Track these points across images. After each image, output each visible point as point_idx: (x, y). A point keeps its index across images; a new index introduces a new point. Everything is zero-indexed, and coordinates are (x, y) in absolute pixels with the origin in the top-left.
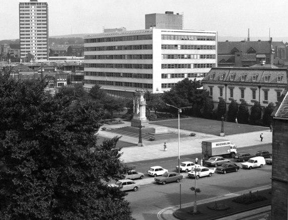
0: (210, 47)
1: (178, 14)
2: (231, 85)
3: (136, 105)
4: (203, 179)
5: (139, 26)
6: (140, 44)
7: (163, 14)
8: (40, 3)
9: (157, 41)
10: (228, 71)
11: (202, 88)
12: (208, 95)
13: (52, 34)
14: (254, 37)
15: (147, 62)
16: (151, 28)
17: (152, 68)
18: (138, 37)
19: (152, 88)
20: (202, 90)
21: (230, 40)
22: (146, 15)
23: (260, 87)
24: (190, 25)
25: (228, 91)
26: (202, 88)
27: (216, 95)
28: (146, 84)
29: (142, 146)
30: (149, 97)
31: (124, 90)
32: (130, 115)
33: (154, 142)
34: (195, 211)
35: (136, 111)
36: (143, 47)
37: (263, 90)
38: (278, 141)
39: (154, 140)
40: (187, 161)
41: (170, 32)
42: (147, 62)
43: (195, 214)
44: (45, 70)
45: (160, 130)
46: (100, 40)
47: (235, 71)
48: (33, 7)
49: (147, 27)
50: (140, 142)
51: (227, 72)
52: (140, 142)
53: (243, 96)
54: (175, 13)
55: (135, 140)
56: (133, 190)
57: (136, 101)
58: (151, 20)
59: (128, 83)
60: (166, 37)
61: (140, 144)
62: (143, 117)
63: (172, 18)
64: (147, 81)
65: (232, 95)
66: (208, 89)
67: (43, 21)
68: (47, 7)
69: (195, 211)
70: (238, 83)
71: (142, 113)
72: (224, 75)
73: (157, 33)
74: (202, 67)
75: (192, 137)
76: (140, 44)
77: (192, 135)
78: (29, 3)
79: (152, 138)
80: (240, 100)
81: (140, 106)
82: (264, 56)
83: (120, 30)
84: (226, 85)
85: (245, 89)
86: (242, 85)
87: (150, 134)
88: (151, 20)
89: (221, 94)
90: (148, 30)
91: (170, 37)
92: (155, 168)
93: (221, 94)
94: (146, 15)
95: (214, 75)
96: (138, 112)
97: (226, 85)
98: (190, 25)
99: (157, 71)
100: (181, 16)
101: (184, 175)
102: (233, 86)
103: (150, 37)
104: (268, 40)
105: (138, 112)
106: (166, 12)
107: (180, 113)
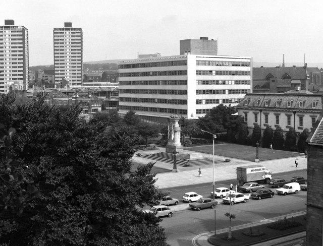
0: (245, 73)
1: (212, 40)
3: (171, 131)
5: (174, 52)
6: (174, 70)
8: (75, 29)
9: (192, 67)
11: (236, 114)
13: (86, 59)
14: (289, 63)
15: (182, 87)
16: (186, 54)
17: (186, 94)
19: (186, 113)
20: (237, 116)
22: (181, 41)
23: (295, 113)
24: (225, 50)
25: (263, 116)
27: (251, 121)
29: (176, 172)
30: (184, 123)
32: (165, 141)
33: (188, 168)
34: (230, 237)
35: (171, 136)
41: (205, 58)
42: (182, 87)
44: (79, 96)
45: (195, 156)
46: (134, 66)
47: (270, 97)
48: (67, 33)
49: (182, 53)
50: (175, 167)
51: (262, 98)
52: (175, 167)
53: (278, 122)
54: (209, 39)
55: (170, 166)
56: (168, 216)
58: (186, 46)
61: (174, 170)
62: (178, 143)
64: (182, 107)
66: (243, 115)
67: (77, 46)
68: (81, 33)
71: (177, 139)
72: (259, 101)
73: (192, 59)
74: (237, 93)
76: (174, 70)
77: (227, 161)
78: (63, 29)
79: (187, 164)
81: (175, 132)
82: (299, 82)
83: (154, 56)
84: (261, 111)
85: (280, 114)
86: (277, 110)
88: (186, 46)
89: (256, 120)
90: (182, 56)
91: (204, 63)
92: (190, 194)
93: (256, 120)
94: (181, 41)
97: (261, 111)
98: (225, 50)
99: (192, 97)
100: (216, 41)
102: (279, 113)
103: (185, 63)
104: (303, 65)
106: (201, 38)
107: (215, 139)
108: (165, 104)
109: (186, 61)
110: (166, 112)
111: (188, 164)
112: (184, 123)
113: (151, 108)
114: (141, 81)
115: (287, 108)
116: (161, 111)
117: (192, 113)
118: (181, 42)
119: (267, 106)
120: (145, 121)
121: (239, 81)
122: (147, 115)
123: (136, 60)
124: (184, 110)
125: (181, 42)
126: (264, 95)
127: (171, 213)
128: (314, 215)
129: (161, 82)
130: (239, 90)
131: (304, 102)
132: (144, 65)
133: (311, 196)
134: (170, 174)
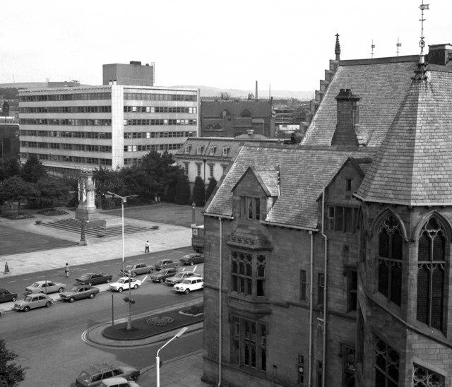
2: (211, 160)
3: (82, 189)
4: (33, 312)
5: (94, 79)
6: (98, 102)
7: (124, 65)
9: (117, 103)
10: (208, 142)
11: (175, 164)
12: (181, 175)
14: (263, 94)
15: (104, 129)
16: (111, 83)
17: (111, 138)
18: (94, 96)
19: (111, 164)
20: (175, 167)
21: (234, 95)
22: (104, 66)
24: (165, 80)
25: (208, 168)
26: (175, 164)
27: (192, 174)
28: (104, 160)
29: (85, 245)
30: (103, 179)
31: (74, 168)
32: (74, 203)
33: (102, 239)
34: (129, 327)
35: (81, 198)
36: (85, 109)
37: (209, 165)
38: (210, 241)
39: (102, 236)
40: (41, 280)
41: (135, 89)
42: (104, 129)
43: (130, 330)
45: (112, 221)
46: (43, 98)
47: (216, 143)
49: (105, 82)
50: (83, 239)
51: (206, 144)
52: (83, 239)
55: (76, 237)
56: (46, 306)
57: (82, 185)
58: (111, 72)
59: (80, 158)
60: (138, 96)
61: (82, 243)
62: (91, 205)
63: (140, 72)
64: (105, 156)
65: (212, 173)
66: (183, 166)
69: (129, 327)
70: (219, 159)
71: (90, 200)
72: (203, 148)
73: (117, 90)
74: (179, 136)
75: (155, 231)
76: (98, 102)
77: (156, 228)
79: (101, 233)
80: (209, 179)
81: (87, 191)
83: (70, 84)
84: (205, 161)
85: (214, 165)
87: (99, 228)
88: (111, 72)
89: (199, 172)
90: (105, 86)
91: (137, 97)
93: (199, 172)
94: (104, 66)
95: (190, 148)
96: (84, 200)
97: (205, 161)
98: (165, 80)
99: (117, 142)
100: (152, 67)
101: (56, 297)
102: (188, 161)
103: (108, 96)
105: (84, 200)
106: (132, 63)
107: (124, 203)
108: (82, 152)
109: (110, 93)
110: (84, 162)
111: (103, 234)
112: (103, 179)
113: (90, 159)
114: (38, 120)
115: (183, 155)
116: (77, 161)
117: (118, 160)
118: (105, 67)
119: (212, 154)
120: (55, 174)
121: (148, 120)
122: (59, 166)
123: (96, 88)
124: (107, 160)
125: (105, 67)
126: (210, 140)
127: (50, 302)
128: (211, 298)
129: (96, 121)
130: (182, 132)
131: (229, 149)
132: (175, 98)
133: (207, 275)
134: (77, 248)
